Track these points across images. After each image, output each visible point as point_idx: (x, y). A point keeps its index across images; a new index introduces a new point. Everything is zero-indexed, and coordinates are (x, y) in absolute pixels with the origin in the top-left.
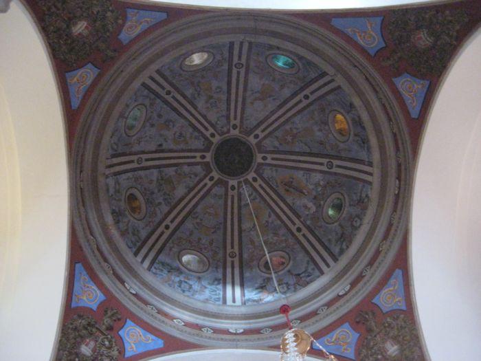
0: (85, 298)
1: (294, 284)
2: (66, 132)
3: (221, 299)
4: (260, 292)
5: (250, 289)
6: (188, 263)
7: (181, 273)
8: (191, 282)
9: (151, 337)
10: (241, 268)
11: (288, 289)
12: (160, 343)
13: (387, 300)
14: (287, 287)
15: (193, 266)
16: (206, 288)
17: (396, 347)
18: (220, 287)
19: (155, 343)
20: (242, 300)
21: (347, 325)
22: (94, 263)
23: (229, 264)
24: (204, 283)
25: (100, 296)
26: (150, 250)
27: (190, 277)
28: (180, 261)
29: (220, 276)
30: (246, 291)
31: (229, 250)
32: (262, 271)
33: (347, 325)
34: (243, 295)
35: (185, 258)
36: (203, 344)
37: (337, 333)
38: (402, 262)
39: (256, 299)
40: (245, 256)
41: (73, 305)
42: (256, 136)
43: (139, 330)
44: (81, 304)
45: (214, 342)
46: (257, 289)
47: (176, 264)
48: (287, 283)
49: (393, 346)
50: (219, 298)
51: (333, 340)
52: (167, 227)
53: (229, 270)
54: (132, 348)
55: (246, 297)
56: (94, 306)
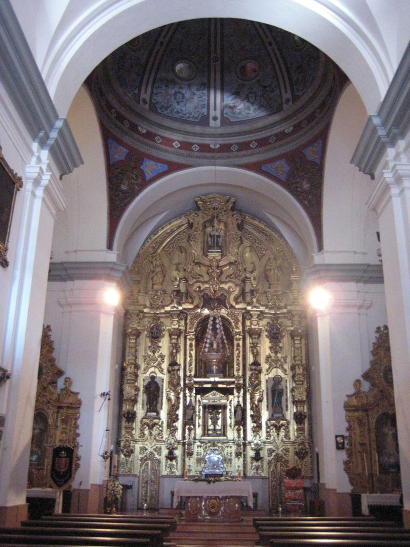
0: (117, 156)
1: (261, 96)
2: (105, 154)
3: (206, 106)
4: (234, 98)
5: (228, 94)
6: (180, 71)
7: (176, 84)
8: (183, 91)
9: (159, 164)
10: (222, 71)
11: (256, 100)
12: (166, 167)
13: (310, 154)
14: (255, 98)
15: (184, 75)
16: (194, 94)
17: (308, 185)
18: (205, 92)
19: (162, 168)
20: (221, 106)
21: (284, 160)
22: (118, 135)
23: (212, 69)
24: (194, 89)
25: (125, 151)
26: (150, 73)
27: (183, 86)
28: (173, 70)
29: (206, 81)
30: (225, 96)
31: (213, 55)
32: (238, 77)
33: (284, 160)
34: (222, 100)
35: (179, 67)
36: (189, 163)
37: (277, 163)
38: (323, 137)
39: (231, 105)
40: (226, 59)
41: (111, 163)
42: (215, 119)
43: (152, 163)
44: (117, 160)
45: (199, 161)
46: (233, 94)
47: (171, 76)
48: (255, 93)
49: (306, 184)
50: (204, 105)
51: (274, 167)
52: (162, 43)
53: (212, 74)
54: (149, 174)
55: (225, 103)
56: (123, 158)
